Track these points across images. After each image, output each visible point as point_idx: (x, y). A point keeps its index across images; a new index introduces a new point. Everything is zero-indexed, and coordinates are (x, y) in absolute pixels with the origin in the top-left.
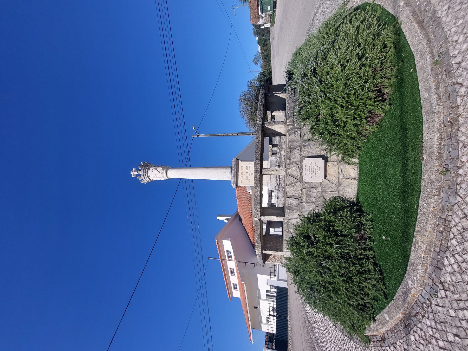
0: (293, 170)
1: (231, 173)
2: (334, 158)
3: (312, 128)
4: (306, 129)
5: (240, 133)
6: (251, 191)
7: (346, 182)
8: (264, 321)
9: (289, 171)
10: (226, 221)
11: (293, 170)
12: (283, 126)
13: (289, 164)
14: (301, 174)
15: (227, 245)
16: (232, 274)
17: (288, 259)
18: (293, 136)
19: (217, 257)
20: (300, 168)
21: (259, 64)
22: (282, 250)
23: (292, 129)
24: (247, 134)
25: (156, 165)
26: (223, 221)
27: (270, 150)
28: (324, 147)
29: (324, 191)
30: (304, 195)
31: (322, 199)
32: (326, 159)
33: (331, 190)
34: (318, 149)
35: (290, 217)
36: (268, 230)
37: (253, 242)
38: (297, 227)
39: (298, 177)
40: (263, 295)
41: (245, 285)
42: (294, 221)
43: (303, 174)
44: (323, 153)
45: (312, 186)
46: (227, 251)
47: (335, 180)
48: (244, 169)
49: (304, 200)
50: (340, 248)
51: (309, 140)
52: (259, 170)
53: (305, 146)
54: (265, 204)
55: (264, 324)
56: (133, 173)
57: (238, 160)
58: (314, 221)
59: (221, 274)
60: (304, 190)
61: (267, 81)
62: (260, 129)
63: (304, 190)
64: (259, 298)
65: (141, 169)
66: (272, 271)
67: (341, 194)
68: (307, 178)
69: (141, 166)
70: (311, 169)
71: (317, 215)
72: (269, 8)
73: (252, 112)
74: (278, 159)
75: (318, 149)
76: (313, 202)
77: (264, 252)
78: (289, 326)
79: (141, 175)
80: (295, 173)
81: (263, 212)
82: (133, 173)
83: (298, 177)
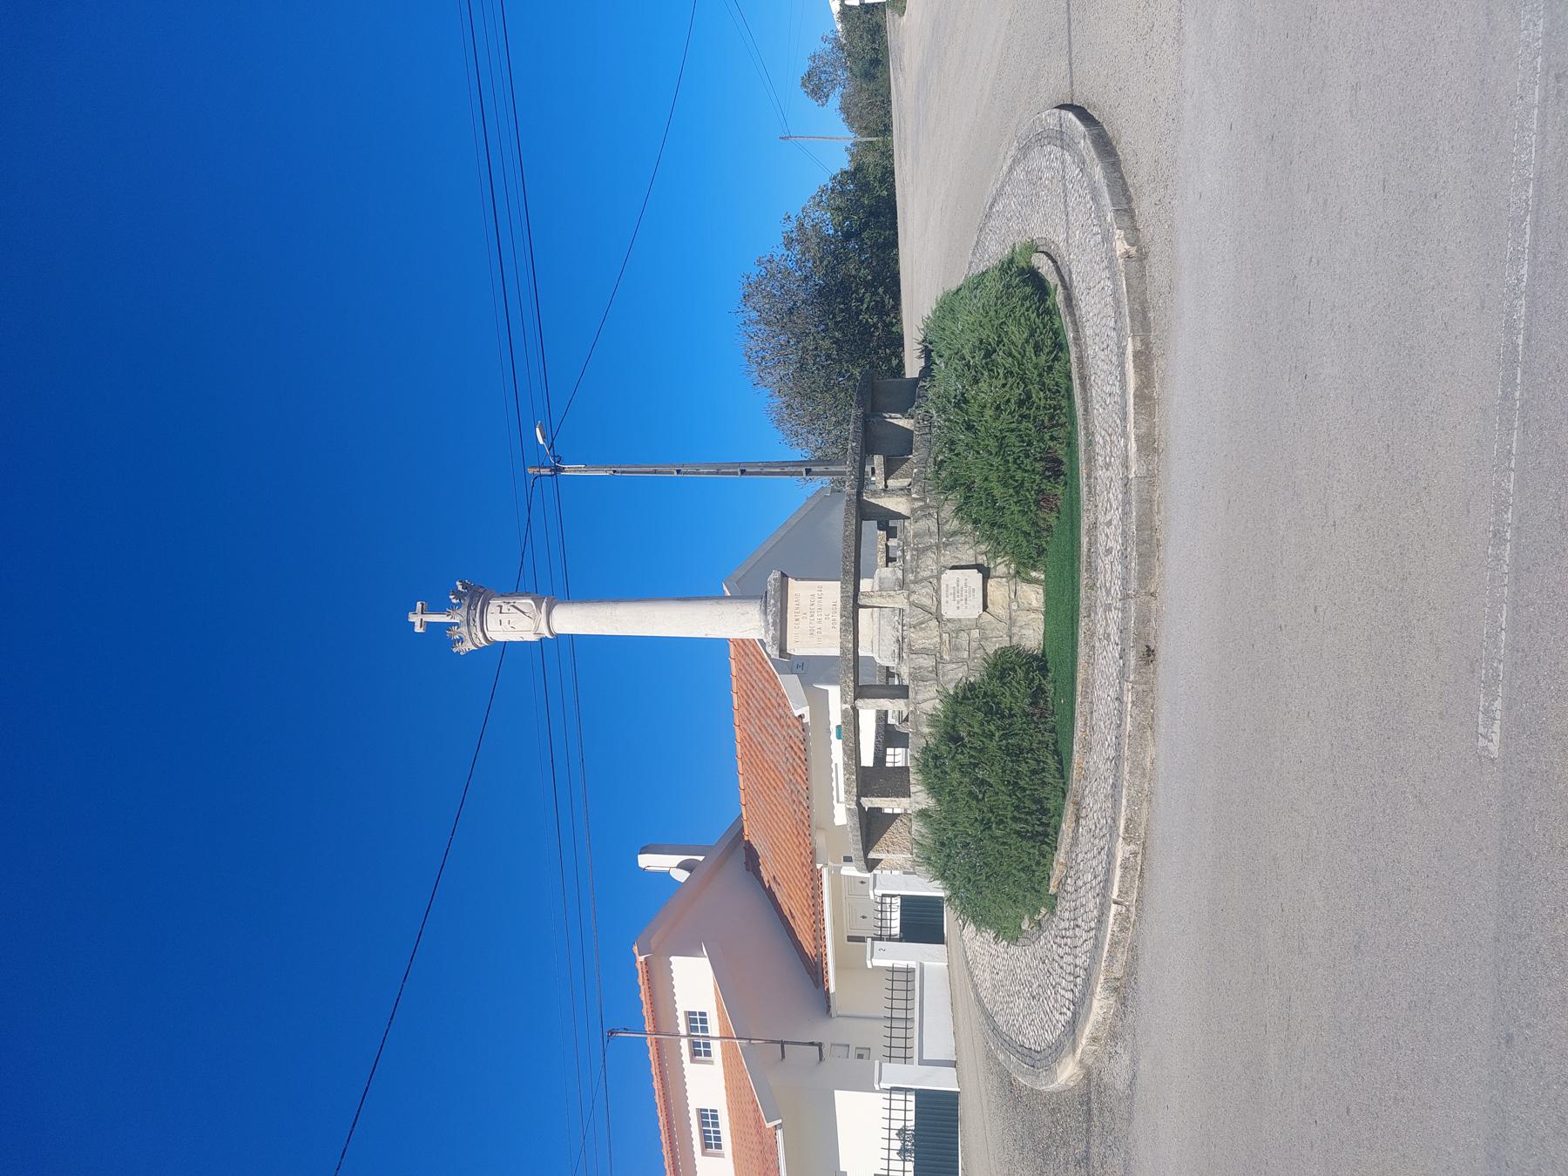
0: (923, 595)
1: (765, 613)
2: (1002, 569)
3: (959, 509)
4: (948, 509)
5: (754, 464)
6: (805, 710)
7: (1023, 618)
9: (914, 597)
10: (682, 876)
12: (903, 500)
13: (915, 582)
14: (939, 602)
15: (693, 983)
16: (706, 1146)
17: (923, 814)
18: (923, 524)
19: (618, 1051)
20: (937, 591)
21: (835, 101)
22: (906, 793)
23: (921, 508)
24: (784, 468)
25: (513, 590)
26: (666, 875)
27: (881, 547)
28: (983, 547)
29: (984, 637)
30: (946, 648)
31: (980, 653)
32: (986, 573)
33: (996, 633)
34: (971, 552)
35: (920, 697)
36: (880, 757)
37: (808, 947)
38: (933, 720)
39: (934, 610)
41: (779, 1132)
42: (927, 707)
43: (943, 600)
44: (982, 559)
45: (960, 627)
47: (1003, 613)
48: (805, 602)
49: (946, 657)
51: (954, 534)
52: (851, 594)
53: (946, 545)
56: (418, 620)
57: (784, 575)
58: (965, 697)
60: (945, 636)
61: (873, 213)
62: (854, 506)
63: (945, 636)
65: (460, 605)
66: (895, 1042)
67: (1015, 640)
68: (949, 611)
69: (458, 595)
70: (957, 593)
71: (972, 687)
74: (900, 574)
75: (971, 552)
76: (963, 661)
77: (868, 803)
80: (927, 602)
82: (418, 620)
83: (934, 610)
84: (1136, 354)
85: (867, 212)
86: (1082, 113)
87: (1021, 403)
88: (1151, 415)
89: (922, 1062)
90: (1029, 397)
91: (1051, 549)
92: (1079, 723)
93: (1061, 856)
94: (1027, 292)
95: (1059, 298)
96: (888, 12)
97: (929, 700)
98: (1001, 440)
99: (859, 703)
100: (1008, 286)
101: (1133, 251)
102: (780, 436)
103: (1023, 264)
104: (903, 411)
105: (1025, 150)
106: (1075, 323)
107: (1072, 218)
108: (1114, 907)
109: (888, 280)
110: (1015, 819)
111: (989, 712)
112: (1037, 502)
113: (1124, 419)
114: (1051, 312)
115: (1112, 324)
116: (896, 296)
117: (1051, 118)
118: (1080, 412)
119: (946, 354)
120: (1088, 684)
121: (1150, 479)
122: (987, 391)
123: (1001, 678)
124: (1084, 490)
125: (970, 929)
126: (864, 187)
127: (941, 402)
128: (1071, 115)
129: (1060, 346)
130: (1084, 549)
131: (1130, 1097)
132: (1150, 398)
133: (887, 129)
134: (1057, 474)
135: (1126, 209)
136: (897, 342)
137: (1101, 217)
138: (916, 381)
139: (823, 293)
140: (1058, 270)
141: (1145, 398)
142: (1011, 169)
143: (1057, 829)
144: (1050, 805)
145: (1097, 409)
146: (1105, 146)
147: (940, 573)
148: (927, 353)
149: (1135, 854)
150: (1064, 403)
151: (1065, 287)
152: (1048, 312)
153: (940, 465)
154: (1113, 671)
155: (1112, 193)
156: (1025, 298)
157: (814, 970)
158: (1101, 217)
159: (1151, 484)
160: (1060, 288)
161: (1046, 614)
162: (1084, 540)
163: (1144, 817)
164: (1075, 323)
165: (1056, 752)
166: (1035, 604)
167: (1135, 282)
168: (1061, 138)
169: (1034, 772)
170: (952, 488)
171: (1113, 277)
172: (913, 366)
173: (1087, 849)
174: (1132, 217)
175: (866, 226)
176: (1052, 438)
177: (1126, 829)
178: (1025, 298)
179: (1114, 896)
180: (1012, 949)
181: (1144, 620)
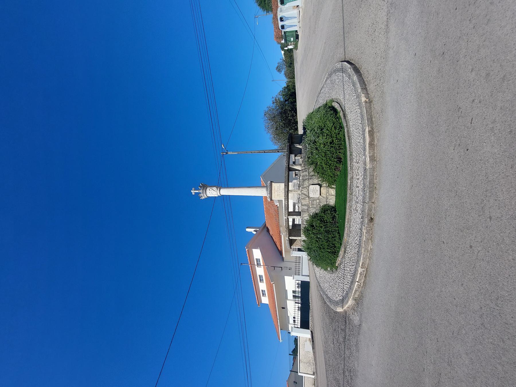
2: (325, 185)
4: (311, 169)
6: (278, 204)
7: (330, 197)
8: (291, 321)
10: (255, 233)
11: (305, 191)
15: (257, 254)
16: (261, 281)
17: (304, 241)
18: (305, 173)
19: (245, 266)
20: (308, 190)
21: (283, 72)
29: (320, 202)
32: (321, 186)
38: (307, 221)
40: (290, 295)
42: (306, 218)
44: (320, 182)
45: (314, 199)
46: (257, 259)
47: (325, 196)
48: (276, 188)
50: (325, 228)
51: (313, 176)
54: (291, 209)
55: (291, 324)
57: (271, 182)
59: (252, 280)
61: (291, 95)
64: (286, 298)
68: (311, 195)
69: (201, 187)
70: (313, 190)
71: (317, 214)
72: (292, 39)
73: (277, 128)
76: (315, 208)
77: (290, 238)
78: (311, 309)
79: (201, 193)
80: (306, 193)
81: (290, 214)
84: (369, 132)
85: (290, 94)
86: (348, 62)
87: (331, 143)
88: (374, 150)
89: (302, 275)
90: (333, 141)
91: (337, 180)
92: (346, 229)
93: (339, 259)
94: (332, 112)
95: (341, 114)
96: (294, 50)
97: (306, 217)
98: (325, 153)
99: (289, 217)
100: (326, 111)
101: (367, 100)
102: (272, 143)
103: (330, 105)
104: (299, 143)
105: (330, 75)
106: (346, 121)
107: (345, 92)
108: (357, 283)
109: (294, 109)
110: (327, 248)
111: (321, 221)
112: (335, 169)
113: (365, 150)
114: (339, 118)
115: (360, 122)
116: (296, 113)
117: (339, 65)
118: (348, 146)
119: (310, 129)
120: (350, 220)
121: (373, 169)
122: (321, 140)
123: (324, 212)
124: (349, 168)
125: (315, 266)
126: (289, 90)
127: (309, 142)
128: (345, 63)
129: (341, 127)
130: (349, 184)
131: (360, 325)
132: (374, 145)
133: (294, 78)
134: (340, 162)
135: (364, 88)
136: (296, 123)
137: (356, 90)
138: (302, 135)
139: (281, 113)
140: (340, 106)
141: (372, 145)
142: (326, 81)
143: (338, 252)
144: (337, 245)
145: (354, 146)
146: (357, 70)
147: (309, 186)
148: (304, 129)
149: (364, 271)
150: (343, 143)
151: (343, 111)
152: (338, 118)
153: (309, 158)
154: (359, 221)
155: (360, 84)
156: (331, 114)
157: (281, 253)
158: (356, 90)
159: (374, 170)
160: (341, 111)
161: (336, 196)
162: (349, 181)
163: (367, 262)
164: (346, 121)
165: (339, 233)
166: (333, 194)
167: (368, 110)
168: (343, 70)
169: (333, 237)
170: (312, 164)
171: (361, 108)
172: (301, 131)
173: (347, 255)
174: (367, 90)
175: (289, 98)
176: (339, 152)
177: (362, 265)
178: (331, 114)
179: (357, 280)
180: (325, 272)
181: (370, 210)
